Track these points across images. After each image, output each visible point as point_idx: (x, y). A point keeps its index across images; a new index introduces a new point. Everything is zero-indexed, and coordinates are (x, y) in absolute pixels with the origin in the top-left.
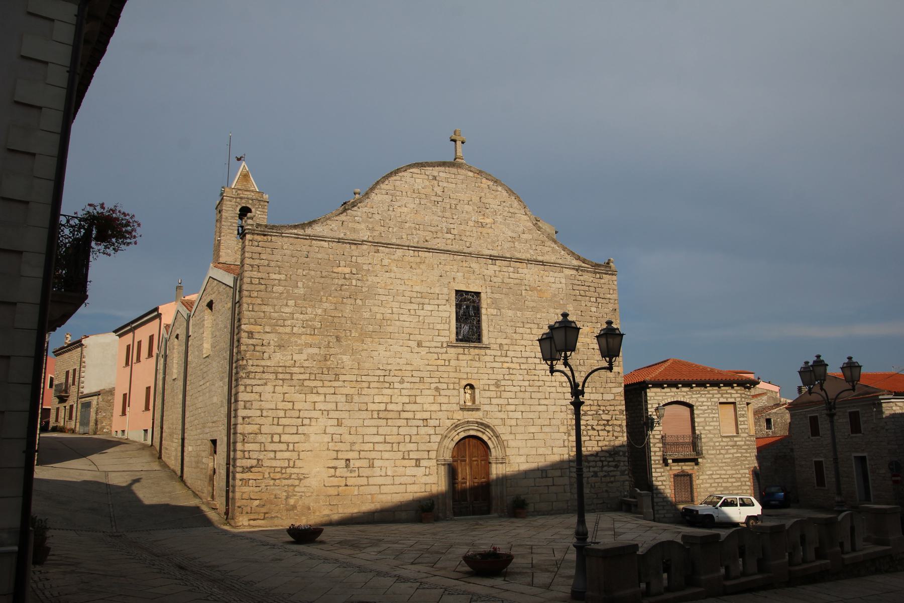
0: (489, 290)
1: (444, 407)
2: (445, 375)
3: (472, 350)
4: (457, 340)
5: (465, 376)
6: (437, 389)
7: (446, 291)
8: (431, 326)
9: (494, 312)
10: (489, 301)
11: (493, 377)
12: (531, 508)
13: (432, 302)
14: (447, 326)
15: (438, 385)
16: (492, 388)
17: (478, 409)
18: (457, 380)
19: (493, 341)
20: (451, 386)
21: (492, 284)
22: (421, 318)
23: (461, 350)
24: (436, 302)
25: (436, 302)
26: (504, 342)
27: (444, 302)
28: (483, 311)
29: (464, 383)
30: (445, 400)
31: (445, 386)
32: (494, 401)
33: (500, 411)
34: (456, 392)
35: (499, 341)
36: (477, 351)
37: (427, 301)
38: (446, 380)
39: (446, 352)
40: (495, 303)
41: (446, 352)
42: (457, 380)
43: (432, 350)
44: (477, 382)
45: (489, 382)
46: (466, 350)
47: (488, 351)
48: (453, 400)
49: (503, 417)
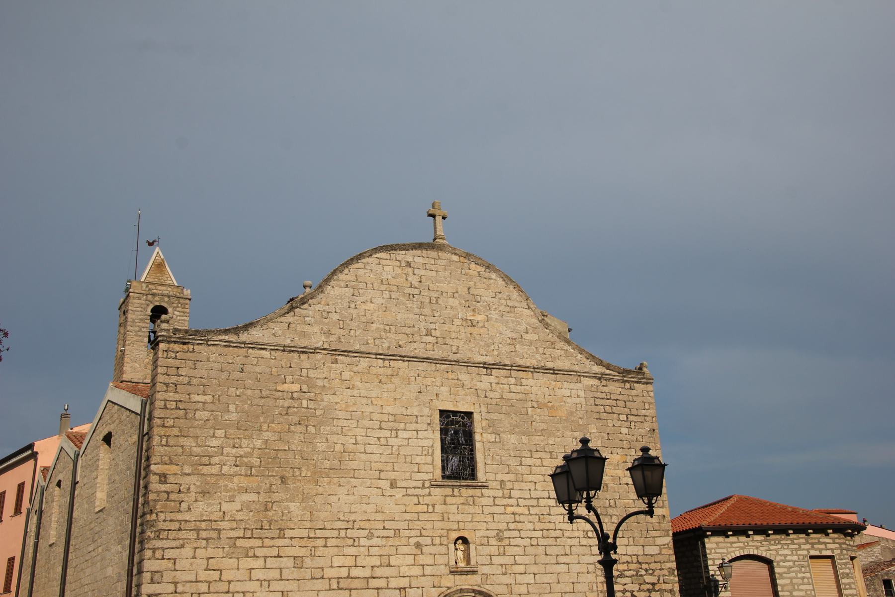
0: (484, 409)
1: (428, 570)
2: (429, 525)
3: (463, 490)
4: (443, 477)
5: (455, 527)
7: (426, 411)
8: (408, 460)
9: (492, 438)
10: (485, 423)
13: (408, 426)
14: (429, 459)
16: (493, 541)
17: (474, 572)
18: (444, 533)
19: (491, 477)
20: (437, 541)
21: (488, 400)
22: (395, 449)
23: (448, 491)
24: (414, 426)
25: (414, 426)
26: (506, 477)
27: (425, 426)
28: (477, 437)
29: (455, 535)
32: (496, 560)
33: (504, 574)
34: (443, 549)
35: (500, 477)
36: (470, 492)
37: (402, 426)
38: (430, 533)
39: (430, 495)
40: (492, 426)
41: (430, 495)
43: (410, 492)
45: (489, 533)
46: (456, 490)
47: (485, 492)
48: (441, 560)
49: (508, 582)
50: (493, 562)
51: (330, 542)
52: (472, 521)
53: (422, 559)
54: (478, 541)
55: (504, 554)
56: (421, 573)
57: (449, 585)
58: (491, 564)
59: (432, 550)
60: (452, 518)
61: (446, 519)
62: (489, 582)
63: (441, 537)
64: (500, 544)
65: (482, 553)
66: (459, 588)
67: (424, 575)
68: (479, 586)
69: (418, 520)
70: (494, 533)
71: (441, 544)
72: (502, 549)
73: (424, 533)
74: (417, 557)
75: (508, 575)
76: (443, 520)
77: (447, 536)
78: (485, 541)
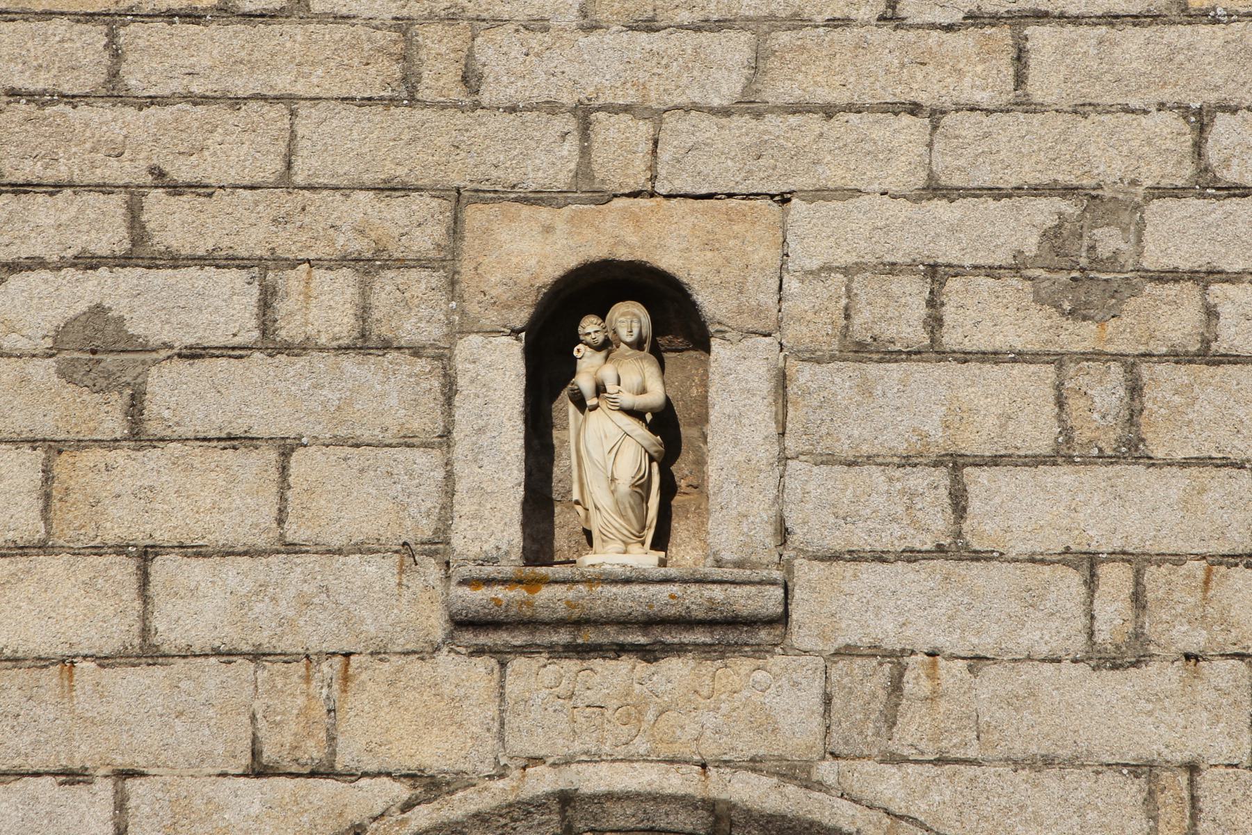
1: (197, 604)
2: (235, 149)
5: (550, 159)
6: (94, 348)
11: (1019, 149)
12: (1203, 766)
15: (115, 289)
16: (988, 315)
17: (735, 631)
18: (415, 224)
20: (324, 306)
29: (535, 252)
30: (229, 498)
31: (226, 305)
32: (1014, 509)
33: (1128, 656)
34: (388, 394)
38: (249, 226)
42: (415, 224)
44: (753, 239)
45: (947, 231)
48: (350, 499)
49: (1160, 738)
50: (982, 527)
51: (226, 305)
52: (749, 105)
53: (129, 493)
54: (811, 311)
55: (1132, 450)
56: (119, 631)
57: (433, 754)
58: (955, 550)
59: (259, 395)
60: (508, 66)
61: (438, 78)
62: (913, 731)
63: (368, 265)
64: (1081, 336)
65: (851, 435)
66: (543, 782)
67: (149, 653)
68: (794, 773)
69: (113, 91)
70: (1020, 229)
71: (366, 343)
72: (1104, 393)
73: (172, 223)
74: (78, 470)
75: (1163, 676)
76: (407, 93)
77: (446, 263)
78: (900, 312)
